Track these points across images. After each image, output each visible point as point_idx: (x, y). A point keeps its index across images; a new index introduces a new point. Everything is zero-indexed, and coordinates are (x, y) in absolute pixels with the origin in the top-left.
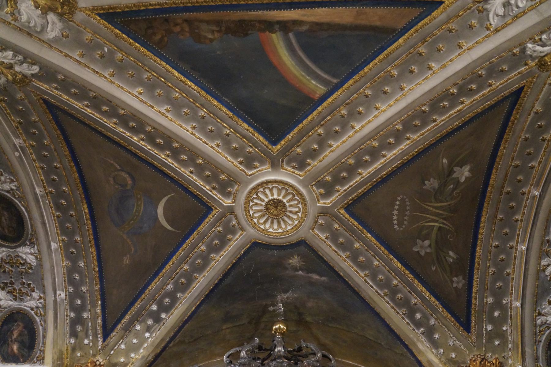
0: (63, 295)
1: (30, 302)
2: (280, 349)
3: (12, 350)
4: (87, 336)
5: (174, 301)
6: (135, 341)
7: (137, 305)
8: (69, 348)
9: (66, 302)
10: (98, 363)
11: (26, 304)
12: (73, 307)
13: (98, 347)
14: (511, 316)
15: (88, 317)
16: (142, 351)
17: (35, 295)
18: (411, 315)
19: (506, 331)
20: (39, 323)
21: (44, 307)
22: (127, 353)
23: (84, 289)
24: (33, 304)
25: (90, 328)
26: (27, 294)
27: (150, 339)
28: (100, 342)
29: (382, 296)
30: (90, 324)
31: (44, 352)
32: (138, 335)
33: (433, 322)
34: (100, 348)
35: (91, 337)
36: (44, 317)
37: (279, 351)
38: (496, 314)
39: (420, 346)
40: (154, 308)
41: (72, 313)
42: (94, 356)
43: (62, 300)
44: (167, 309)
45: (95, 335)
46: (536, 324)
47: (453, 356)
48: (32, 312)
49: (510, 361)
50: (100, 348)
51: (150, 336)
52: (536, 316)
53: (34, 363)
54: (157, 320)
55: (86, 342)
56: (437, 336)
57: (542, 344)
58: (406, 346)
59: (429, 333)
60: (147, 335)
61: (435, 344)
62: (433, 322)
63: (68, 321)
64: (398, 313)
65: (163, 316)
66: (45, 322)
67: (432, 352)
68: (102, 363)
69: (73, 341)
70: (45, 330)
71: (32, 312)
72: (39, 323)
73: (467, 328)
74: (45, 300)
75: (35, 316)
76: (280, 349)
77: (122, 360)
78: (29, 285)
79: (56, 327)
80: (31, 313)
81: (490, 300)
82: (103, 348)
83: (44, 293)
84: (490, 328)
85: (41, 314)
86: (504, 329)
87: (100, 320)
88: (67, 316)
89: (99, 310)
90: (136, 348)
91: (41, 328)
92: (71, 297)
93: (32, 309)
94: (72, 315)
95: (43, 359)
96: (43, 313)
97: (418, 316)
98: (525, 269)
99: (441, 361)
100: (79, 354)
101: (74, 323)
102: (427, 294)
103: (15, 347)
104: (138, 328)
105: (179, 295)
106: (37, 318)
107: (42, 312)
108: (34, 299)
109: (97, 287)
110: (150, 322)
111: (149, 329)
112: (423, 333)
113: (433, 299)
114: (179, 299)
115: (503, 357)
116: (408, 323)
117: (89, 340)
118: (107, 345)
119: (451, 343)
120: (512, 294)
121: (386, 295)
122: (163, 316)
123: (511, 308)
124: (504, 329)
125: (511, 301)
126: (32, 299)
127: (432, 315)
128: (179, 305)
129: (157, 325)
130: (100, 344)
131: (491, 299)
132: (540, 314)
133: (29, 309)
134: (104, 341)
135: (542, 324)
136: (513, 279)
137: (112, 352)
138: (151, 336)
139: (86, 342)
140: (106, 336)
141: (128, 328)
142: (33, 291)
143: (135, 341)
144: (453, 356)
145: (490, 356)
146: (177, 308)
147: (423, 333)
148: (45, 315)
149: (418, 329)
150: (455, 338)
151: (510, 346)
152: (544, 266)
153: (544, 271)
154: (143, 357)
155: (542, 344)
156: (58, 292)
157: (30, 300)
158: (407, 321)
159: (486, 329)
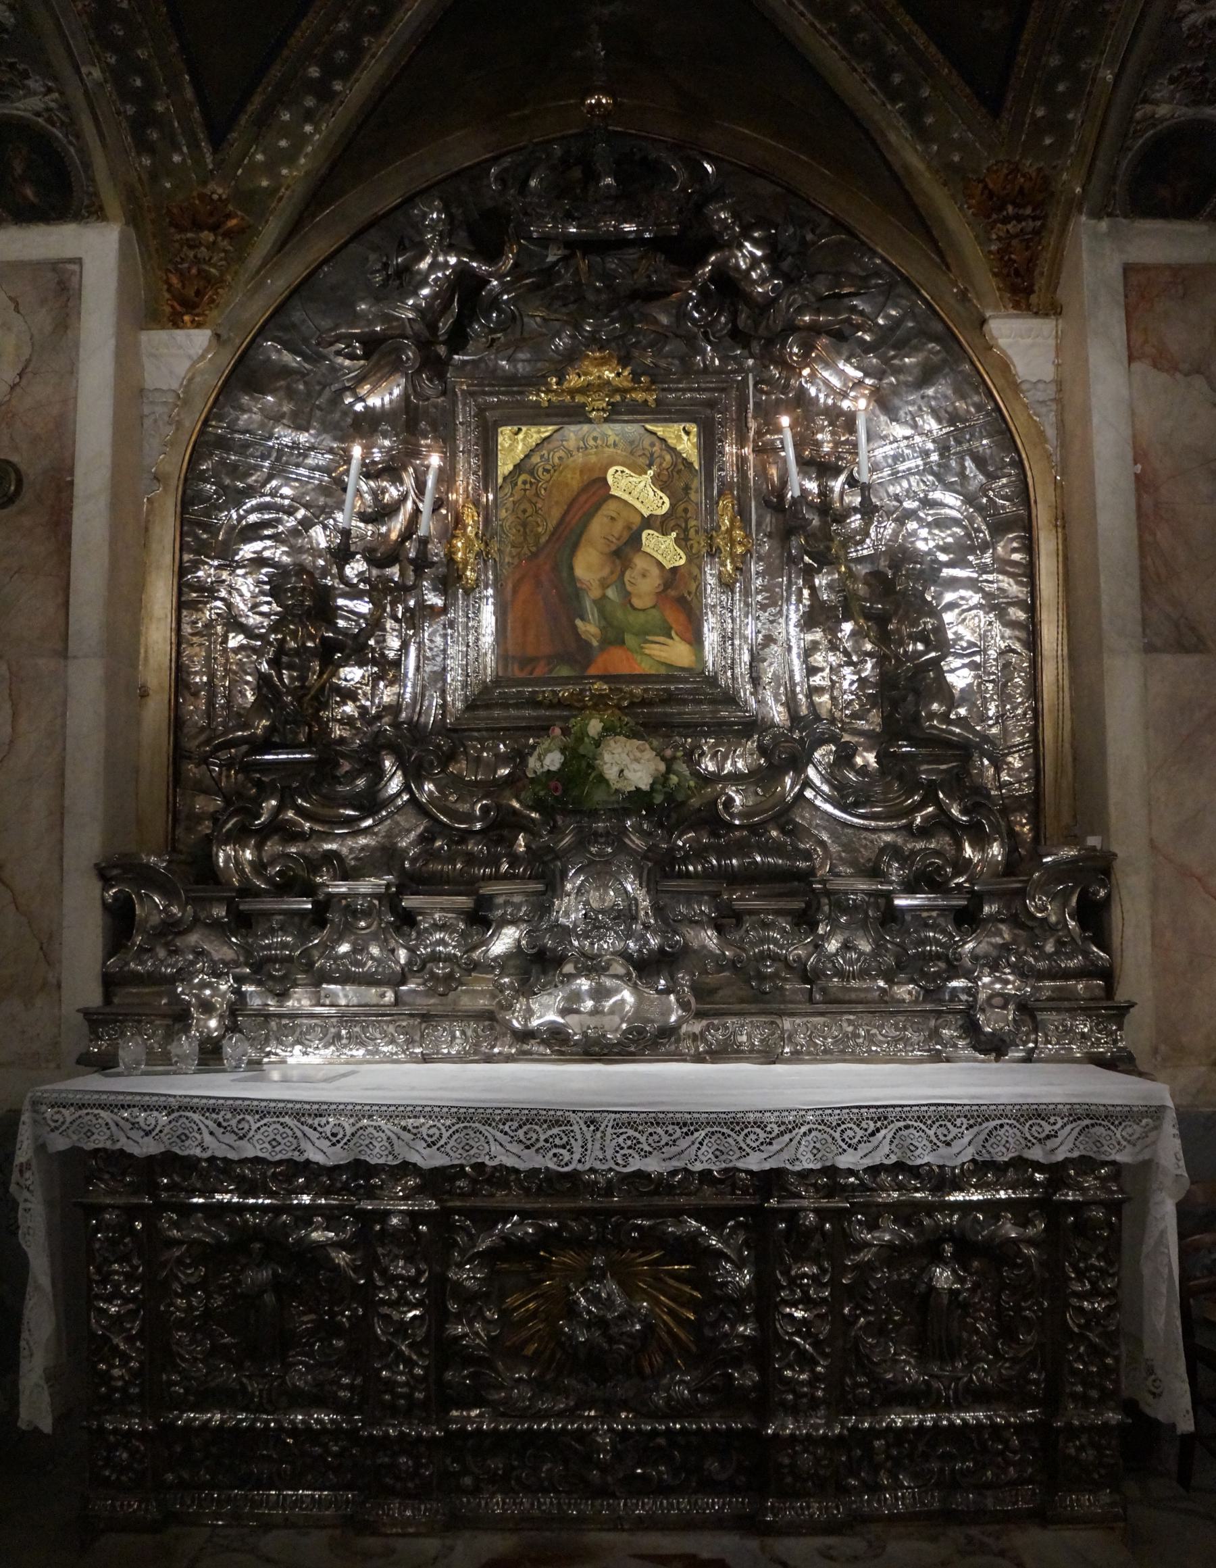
0: (97, 73)
1: (27, 100)
2: (609, 180)
3: (25, 198)
4: (177, 148)
5: (357, 54)
6: (283, 143)
7: (276, 72)
8: (145, 177)
9: (109, 87)
10: (215, 197)
11: (17, 104)
12: (126, 95)
13: (206, 165)
14: (1090, 93)
15: (168, 109)
16: (302, 161)
17: (34, 84)
18: (882, 78)
19: (1073, 121)
20: (65, 141)
21: (66, 107)
22: (270, 168)
23: (142, 54)
24: (36, 103)
25: (179, 131)
26: (12, 84)
27: (317, 137)
28: (208, 155)
29: (823, 36)
30: (176, 124)
31: (96, 194)
32: (285, 130)
33: (926, 92)
34: (211, 167)
35: (185, 149)
36: (71, 126)
37: (608, 186)
38: (1061, 88)
39: (893, 137)
40: (314, 72)
41: (128, 107)
42: (204, 183)
43: (101, 85)
44: (346, 72)
45: (194, 145)
46: (1131, 118)
47: (956, 159)
48: (40, 120)
49: (1065, 176)
50: (211, 167)
51: (315, 129)
52: (1136, 104)
53: (83, 217)
54: (325, 94)
55: (177, 158)
56: (929, 120)
57: (1130, 155)
58: (866, 132)
59: (914, 115)
60: (308, 128)
61: (922, 134)
62: (926, 92)
63: (124, 125)
64: (855, 70)
65: (338, 86)
66: (78, 137)
67: (916, 150)
68: (224, 197)
69: (147, 161)
70: (83, 151)
71: (40, 120)
72: (65, 141)
73: (994, 105)
74: (62, 94)
75: (50, 127)
76: (609, 180)
77: (265, 183)
78: (12, 66)
79: (104, 145)
80: (38, 122)
81: (1055, 61)
82: (219, 165)
83: (55, 79)
84: (1040, 113)
85: (63, 123)
86: (1070, 116)
87: (196, 113)
88: (119, 113)
89: (189, 93)
90: (290, 158)
91: (72, 150)
92: (117, 76)
93: (38, 114)
94: (130, 110)
95: (101, 208)
96: (67, 120)
97: (897, 79)
98: (1143, 11)
99: (929, 167)
100: (168, 185)
101: (139, 125)
102: (921, 40)
103: (29, 192)
104: (286, 117)
105: (366, 39)
106: (54, 130)
107: (63, 118)
108: (35, 94)
109: (174, 47)
110: (310, 102)
111: (309, 116)
112: (902, 112)
113: (933, 49)
114: (369, 48)
115: (1055, 167)
116: (873, 92)
117: (182, 153)
118: (223, 160)
119: (956, 135)
120: (1102, 53)
121: (831, 32)
122: (338, 86)
123: (1094, 80)
124: (1070, 116)
125: (1099, 65)
126: (30, 93)
127: (926, 80)
128: (369, 62)
129: (327, 106)
130: (209, 160)
131: (1057, 57)
132: (1145, 100)
133: (28, 115)
134: (215, 151)
135: (1144, 119)
136: (1113, 24)
137: (240, 172)
138: (317, 130)
139: (177, 158)
140: (217, 142)
141: (264, 121)
142: (28, 77)
143: (283, 143)
144: (956, 159)
145: (1028, 164)
146: (366, 66)
147: (902, 112)
148: (73, 121)
149: (894, 105)
150: (965, 128)
151: (1072, 149)
152: (1181, 12)
153: (1179, 20)
154: (307, 173)
155: (1130, 155)
156: (84, 70)
157: (25, 97)
158: (873, 86)
159: (1033, 114)
